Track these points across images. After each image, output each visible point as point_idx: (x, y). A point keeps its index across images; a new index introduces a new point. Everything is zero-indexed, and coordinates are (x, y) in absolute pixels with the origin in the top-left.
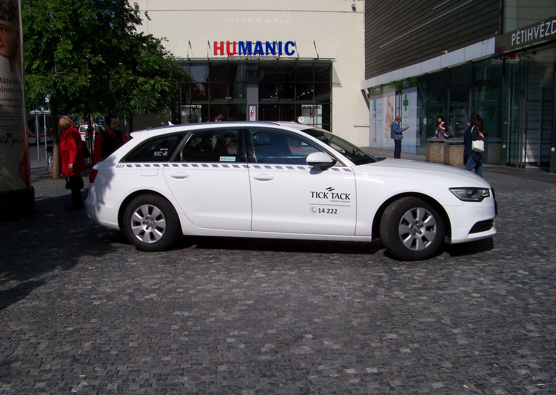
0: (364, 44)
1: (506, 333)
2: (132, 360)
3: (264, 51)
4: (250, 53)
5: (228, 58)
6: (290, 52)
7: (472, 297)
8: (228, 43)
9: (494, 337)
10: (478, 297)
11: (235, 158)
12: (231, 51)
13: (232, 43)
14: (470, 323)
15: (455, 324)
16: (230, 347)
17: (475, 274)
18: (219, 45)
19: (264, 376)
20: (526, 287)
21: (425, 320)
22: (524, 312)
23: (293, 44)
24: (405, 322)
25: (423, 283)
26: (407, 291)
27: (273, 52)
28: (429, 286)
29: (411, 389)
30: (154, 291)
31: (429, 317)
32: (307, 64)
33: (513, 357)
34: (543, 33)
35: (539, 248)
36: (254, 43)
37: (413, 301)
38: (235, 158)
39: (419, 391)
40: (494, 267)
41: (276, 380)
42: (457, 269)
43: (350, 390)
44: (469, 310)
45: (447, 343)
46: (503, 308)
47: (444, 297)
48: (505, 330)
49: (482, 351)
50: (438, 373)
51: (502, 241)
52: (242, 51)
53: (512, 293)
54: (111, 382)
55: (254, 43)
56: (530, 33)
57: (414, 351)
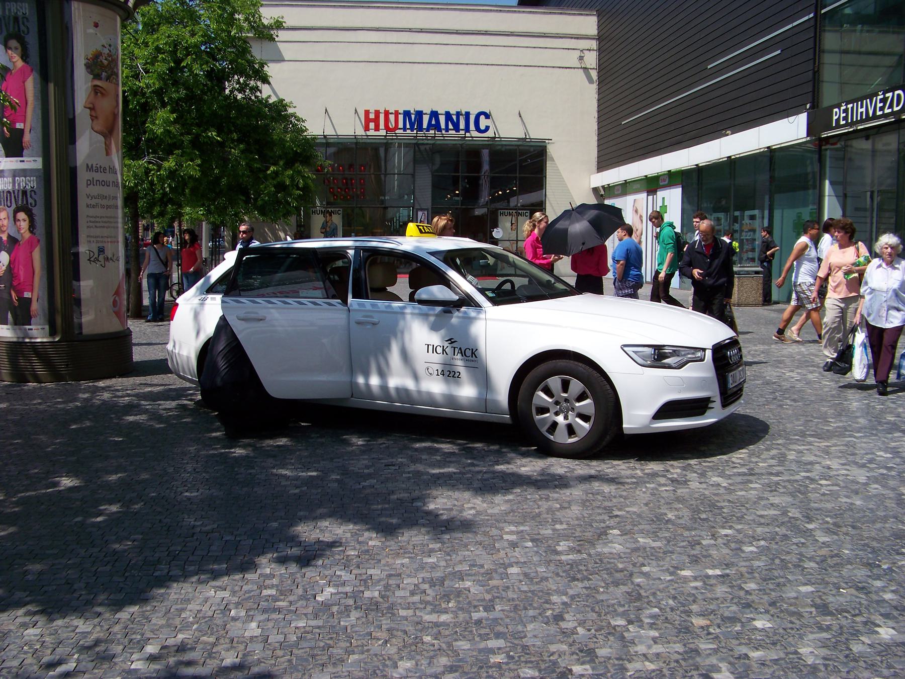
0: (597, 117)
1: (880, 530)
2: (383, 562)
3: (443, 126)
4: (420, 128)
5: (386, 136)
6: (482, 127)
7: (821, 485)
8: (387, 113)
9: (865, 534)
10: (829, 485)
11: (527, 279)
12: (392, 125)
13: (392, 113)
14: (827, 516)
15: (808, 517)
16: (514, 545)
17: (816, 455)
18: (372, 116)
19: (574, 579)
20: (893, 473)
21: (766, 513)
22: (897, 504)
23: (487, 116)
24: (739, 515)
25: (748, 467)
26: (729, 477)
27: (457, 128)
28: (757, 471)
29: (773, 593)
30: (370, 476)
31: (769, 509)
32: (508, 147)
33: (897, 557)
34: (882, 109)
35: (899, 424)
36: (426, 114)
37: (742, 490)
38: (527, 279)
39: (784, 596)
40: (842, 448)
41: (592, 584)
42: (790, 450)
43: (694, 595)
44: (821, 500)
45: (803, 540)
46: (868, 498)
47: (783, 484)
48: (878, 525)
49: (853, 550)
50: (802, 575)
51: (844, 414)
52: (408, 126)
53: (876, 480)
54: (368, 588)
55: (426, 114)
56: (862, 107)
57: (763, 551)
